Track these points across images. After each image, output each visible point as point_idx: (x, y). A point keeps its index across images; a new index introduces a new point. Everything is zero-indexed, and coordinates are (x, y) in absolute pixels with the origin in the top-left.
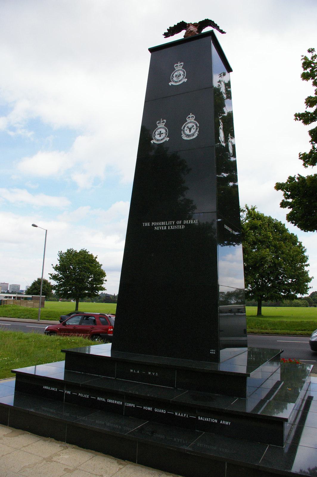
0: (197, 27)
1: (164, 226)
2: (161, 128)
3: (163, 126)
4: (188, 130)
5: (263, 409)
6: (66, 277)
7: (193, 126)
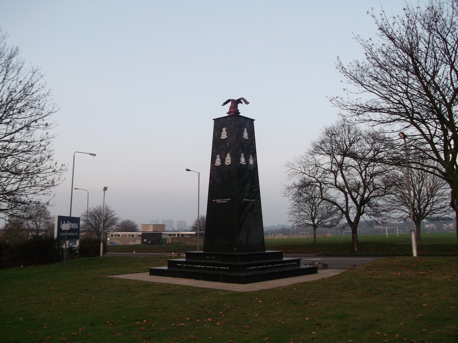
2: (218, 158)
3: (219, 158)
5: (291, 269)
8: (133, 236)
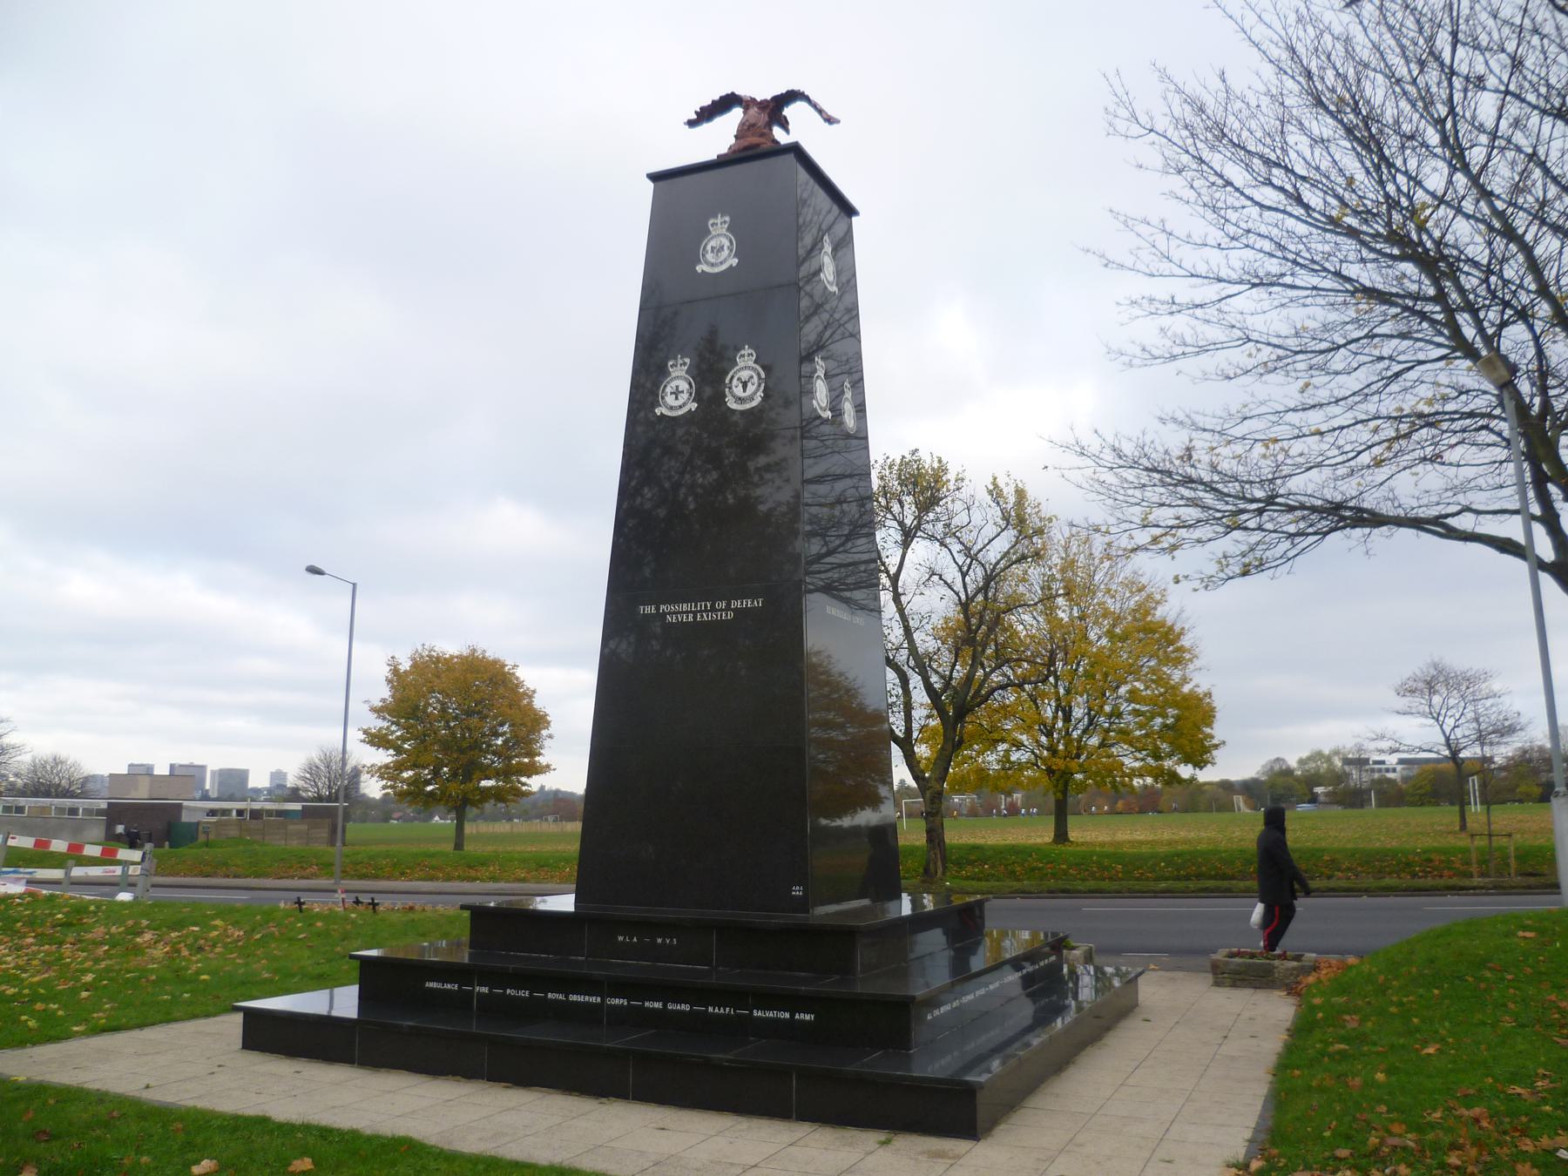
0: (768, 111)
1: (687, 612)
2: (677, 378)
3: (724, 231)
4: (740, 385)
6: (421, 739)
7: (752, 377)
8: (73, 811)
